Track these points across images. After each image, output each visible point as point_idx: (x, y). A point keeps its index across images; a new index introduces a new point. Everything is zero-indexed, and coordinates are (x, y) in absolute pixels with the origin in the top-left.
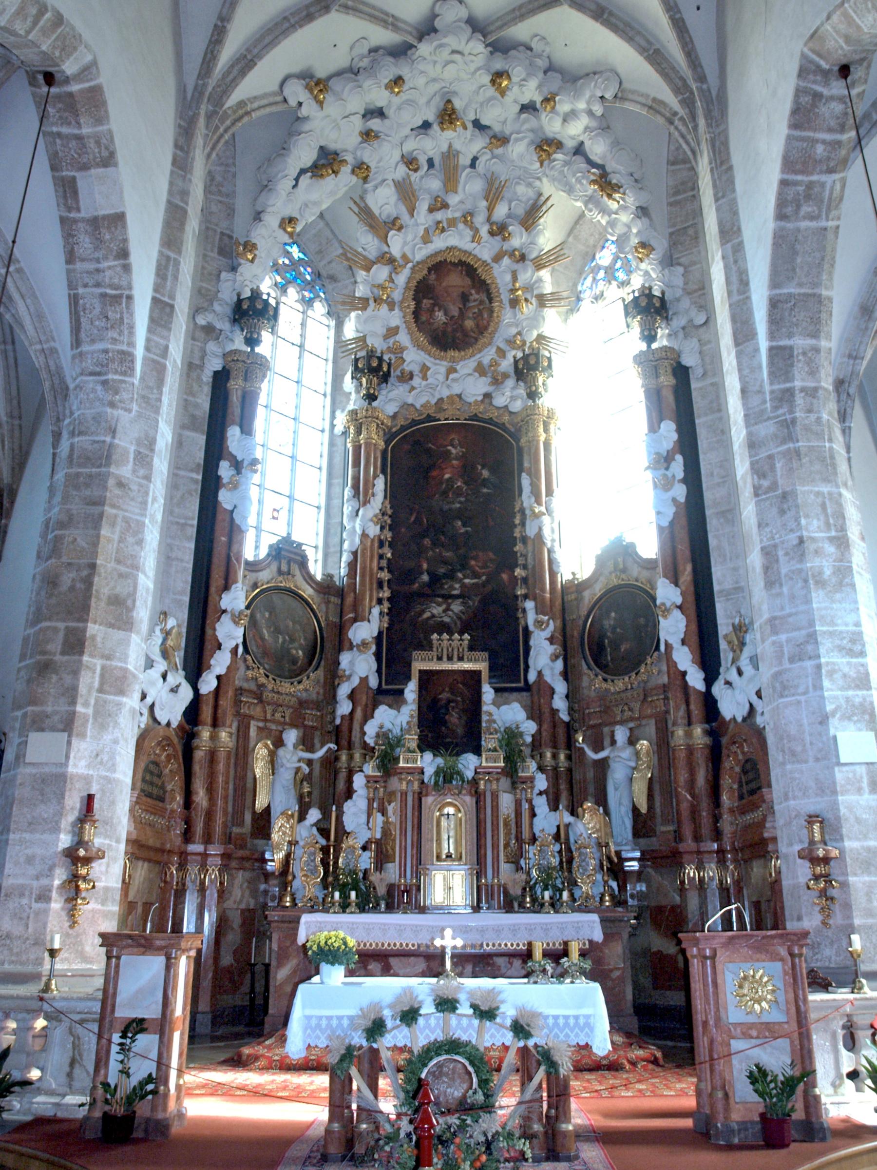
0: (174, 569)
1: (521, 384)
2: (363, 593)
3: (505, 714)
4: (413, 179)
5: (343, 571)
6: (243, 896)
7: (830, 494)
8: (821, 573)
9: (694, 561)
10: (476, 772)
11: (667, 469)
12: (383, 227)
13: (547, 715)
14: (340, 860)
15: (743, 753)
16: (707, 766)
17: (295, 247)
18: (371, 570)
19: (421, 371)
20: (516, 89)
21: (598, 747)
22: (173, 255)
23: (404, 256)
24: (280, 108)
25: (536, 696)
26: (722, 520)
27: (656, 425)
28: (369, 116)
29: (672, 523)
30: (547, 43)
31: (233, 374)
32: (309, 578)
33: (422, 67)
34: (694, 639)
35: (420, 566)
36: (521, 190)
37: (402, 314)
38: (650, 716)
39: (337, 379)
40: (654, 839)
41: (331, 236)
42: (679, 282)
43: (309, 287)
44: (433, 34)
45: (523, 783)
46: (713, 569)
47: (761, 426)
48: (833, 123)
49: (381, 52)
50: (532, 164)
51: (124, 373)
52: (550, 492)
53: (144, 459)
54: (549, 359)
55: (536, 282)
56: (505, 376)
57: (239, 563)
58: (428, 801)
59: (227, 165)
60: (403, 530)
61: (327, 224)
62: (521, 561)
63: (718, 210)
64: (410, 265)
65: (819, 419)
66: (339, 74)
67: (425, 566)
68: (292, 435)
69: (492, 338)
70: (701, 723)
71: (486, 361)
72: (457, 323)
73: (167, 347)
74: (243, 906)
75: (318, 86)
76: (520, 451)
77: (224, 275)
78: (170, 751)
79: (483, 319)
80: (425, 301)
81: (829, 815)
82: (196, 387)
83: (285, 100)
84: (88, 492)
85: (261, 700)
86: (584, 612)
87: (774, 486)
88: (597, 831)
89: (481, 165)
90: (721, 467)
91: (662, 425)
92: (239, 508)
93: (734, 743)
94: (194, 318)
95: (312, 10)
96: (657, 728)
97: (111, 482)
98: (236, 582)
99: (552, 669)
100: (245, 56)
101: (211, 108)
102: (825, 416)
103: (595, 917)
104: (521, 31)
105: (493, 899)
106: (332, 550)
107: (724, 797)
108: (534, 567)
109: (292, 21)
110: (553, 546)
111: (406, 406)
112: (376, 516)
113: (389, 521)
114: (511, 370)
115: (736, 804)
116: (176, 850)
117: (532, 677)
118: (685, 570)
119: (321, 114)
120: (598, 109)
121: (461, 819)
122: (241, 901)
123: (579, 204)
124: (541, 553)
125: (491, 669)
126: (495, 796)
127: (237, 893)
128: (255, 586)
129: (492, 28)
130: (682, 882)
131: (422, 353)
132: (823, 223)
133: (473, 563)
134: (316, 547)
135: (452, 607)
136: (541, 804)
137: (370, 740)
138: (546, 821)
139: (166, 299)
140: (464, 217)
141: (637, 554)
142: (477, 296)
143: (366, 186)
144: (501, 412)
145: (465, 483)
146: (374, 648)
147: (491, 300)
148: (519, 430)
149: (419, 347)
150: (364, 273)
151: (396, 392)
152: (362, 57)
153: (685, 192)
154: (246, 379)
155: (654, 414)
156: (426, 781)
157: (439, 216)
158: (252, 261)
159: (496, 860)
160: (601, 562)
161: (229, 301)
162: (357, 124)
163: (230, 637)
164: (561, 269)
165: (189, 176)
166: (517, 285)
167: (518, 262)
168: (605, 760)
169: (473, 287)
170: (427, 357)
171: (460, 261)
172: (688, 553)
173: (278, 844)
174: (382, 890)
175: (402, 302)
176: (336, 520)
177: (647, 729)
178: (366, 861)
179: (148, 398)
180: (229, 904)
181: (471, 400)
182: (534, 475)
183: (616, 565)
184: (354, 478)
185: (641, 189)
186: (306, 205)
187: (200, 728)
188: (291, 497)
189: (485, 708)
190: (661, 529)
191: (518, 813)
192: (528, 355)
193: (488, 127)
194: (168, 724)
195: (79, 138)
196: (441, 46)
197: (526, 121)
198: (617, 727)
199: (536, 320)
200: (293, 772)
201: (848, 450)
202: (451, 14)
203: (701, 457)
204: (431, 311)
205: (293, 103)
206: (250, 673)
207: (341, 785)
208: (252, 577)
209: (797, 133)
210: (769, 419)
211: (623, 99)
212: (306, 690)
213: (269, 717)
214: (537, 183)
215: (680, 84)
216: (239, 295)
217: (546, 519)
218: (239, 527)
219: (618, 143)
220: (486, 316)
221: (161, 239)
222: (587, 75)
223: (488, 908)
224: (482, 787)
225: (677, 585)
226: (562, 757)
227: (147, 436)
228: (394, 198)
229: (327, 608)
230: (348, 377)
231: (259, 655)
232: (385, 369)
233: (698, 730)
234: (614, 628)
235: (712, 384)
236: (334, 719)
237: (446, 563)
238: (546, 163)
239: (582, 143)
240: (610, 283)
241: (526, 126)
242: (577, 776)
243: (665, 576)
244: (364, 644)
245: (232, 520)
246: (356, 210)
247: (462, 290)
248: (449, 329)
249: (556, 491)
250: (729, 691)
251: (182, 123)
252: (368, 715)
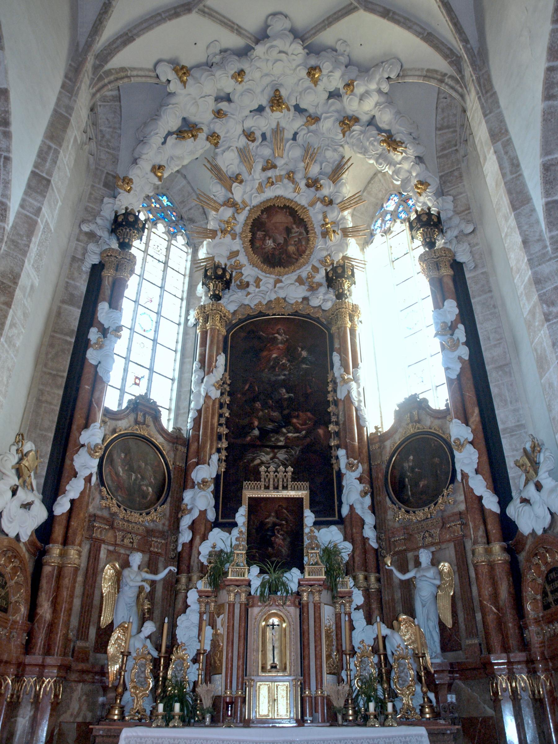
0: (43, 409)
1: (331, 290)
2: (205, 442)
4: (251, 148)
5: (189, 426)
6: (80, 709)
9: (480, 404)
10: (300, 585)
11: (452, 334)
12: (229, 180)
13: (358, 539)
14: (170, 672)
15: (546, 563)
16: (509, 580)
17: (165, 198)
18: (212, 424)
19: (255, 282)
20: (325, 79)
21: (404, 569)
25: (350, 526)
26: (500, 373)
27: (441, 304)
28: (219, 100)
29: (459, 376)
30: (347, 45)
31: (107, 266)
32: (162, 431)
33: (258, 64)
34: (486, 468)
35: (253, 423)
36: (329, 154)
37: (241, 242)
38: (449, 541)
40: (460, 652)
41: (191, 191)
42: (450, 206)
43: (173, 225)
44: (266, 39)
45: (342, 597)
46: (497, 412)
47: (544, 265)
49: (229, 52)
50: (336, 135)
52: (356, 365)
55: (341, 219)
56: (320, 285)
58: (255, 611)
59: (114, 128)
60: (239, 396)
61: (189, 183)
62: (334, 419)
63: (487, 122)
64: (248, 208)
67: (256, 423)
68: (154, 324)
69: (309, 259)
70: (499, 541)
71: (304, 275)
72: (282, 248)
73: (40, 209)
74: (80, 719)
75: (183, 71)
76: (331, 337)
77: (106, 200)
78: (17, 563)
79: (302, 246)
80: (259, 233)
82: (76, 274)
83: (158, 77)
85: (112, 527)
86: (386, 457)
88: (413, 642)
89: (300, 138)
90: (495, 332)
91: (446, 303)
92: (102, 363)
93: (536, 555)
94: (80, 226)
95: (178, 10)
96: (456, 551)
98: (94, 421)
99: (362, 504)
100: (127, 34)
101: (97, 62)
103: (422, 731)
104: (327, 37)
105: (316, 711)
106: (182, 411)
107: (529, 607)
108: (345, 421)
109: (163, 16)
110: (359, 405)
111: (243, 306)
112: (217, 382)
113: (228, 389)
114: (324, 281)
115: (541, 615)
116: (14, 661)
117: (345, 511)
118: (474, 412)
120: (385, 87)
121: (285, 629)
122: (78, 714)
123: (372, 161)
124: (350, 410)
125: (312, 494)
126: (317, 608)
127: (75, 706)
128: (114, 431)
130: (496, 693)
131: (256, 269)
133: (295, 420)
134: (169, 410)
135: (278, 455)
136: (359, 618)
137: (204, 559)
138: (364, 634)
139: (44, 175)
140: (288, 174)
141: (429, 407)
142: (297, 230)
143: (217, 150)
144: (316, 310)
145: (289, 361)
146: (212, 487)
147: (307, 232)
148: (330, 323)
149: (254, 265)
150: (214, 213)
151: (236, 296)
152: (215, 55)
153: (450, 148)
154: (117, 270)
155: (438, 296)
156: (252, 593)
157: (270, 173)
158: (129, 191)
159: (319, 669)
160: (399, 415)
161: (109, 218)
162: (211, 104)
163: (85, 467)
164: (358, 215)
165: (74, 98)
166: (327, 220)
167: (327, 205)
169: (295, 223)
170: (260, 272)
171: (285, 205)
173: (114, 656)
174: (207, 703)
175: (241, 234)
176: (186, 389)
177: (447, 552)
178: (193, 673)
179: (18, 243)
180: (66, 717)
181: (292, 302)
182: (343, 351)
183: (411, 418)
184: (201, 355)
185: (418, 144)
186: (172, 158)
187: (51, 545)
188: (151, 370)
189: (306, 530)
190: (450, 382)
191: (338, 627)
192: (336, 267)
193: (306, 110)
194: (18, 537)
196: (272, 47)
197: (333, 104)
198: (422, 550)
199: (343, 246)
200: (137, 590)
202: (278, 25)
203: (478, 326)
204: (263, 240)
205: (163, 79)
206: (104, 503)
208: (111, 424)
210: (551, 259)
211: (404, 76)
212: (153, 521)
213: (118, 542)
214: (341, 149)
215: (448, 52)
216: (116, 212)
217: (353, 385)
218: (101, 378)
219: (400, 113)
220: (304, 243)
221: (46, 133)
222: (377, 65)
223: (312, 722)
224: (305, 599)
225: (467, 425)
226: (373, 579)
227: (12, 272)
228: (237, 161)
229: (175, 455)
230: (200, 286)
231: (113, 489)
232: (228, 277)
233: (497, 547)
234: (412, 469)
235: (482, 273)
236: (177, 546)
237: (272, 421)
238: (347, 133)
239: (374, 116)
240: (395, 221)
241: (333, 108)
242: (386, 597)
243: (457, 417)
244: (204, 482)
245: (96, 372)
247: (285, 225)
248: (277, 252)
249: (361, 365)
250: (527, 508)
251: (73, 64)
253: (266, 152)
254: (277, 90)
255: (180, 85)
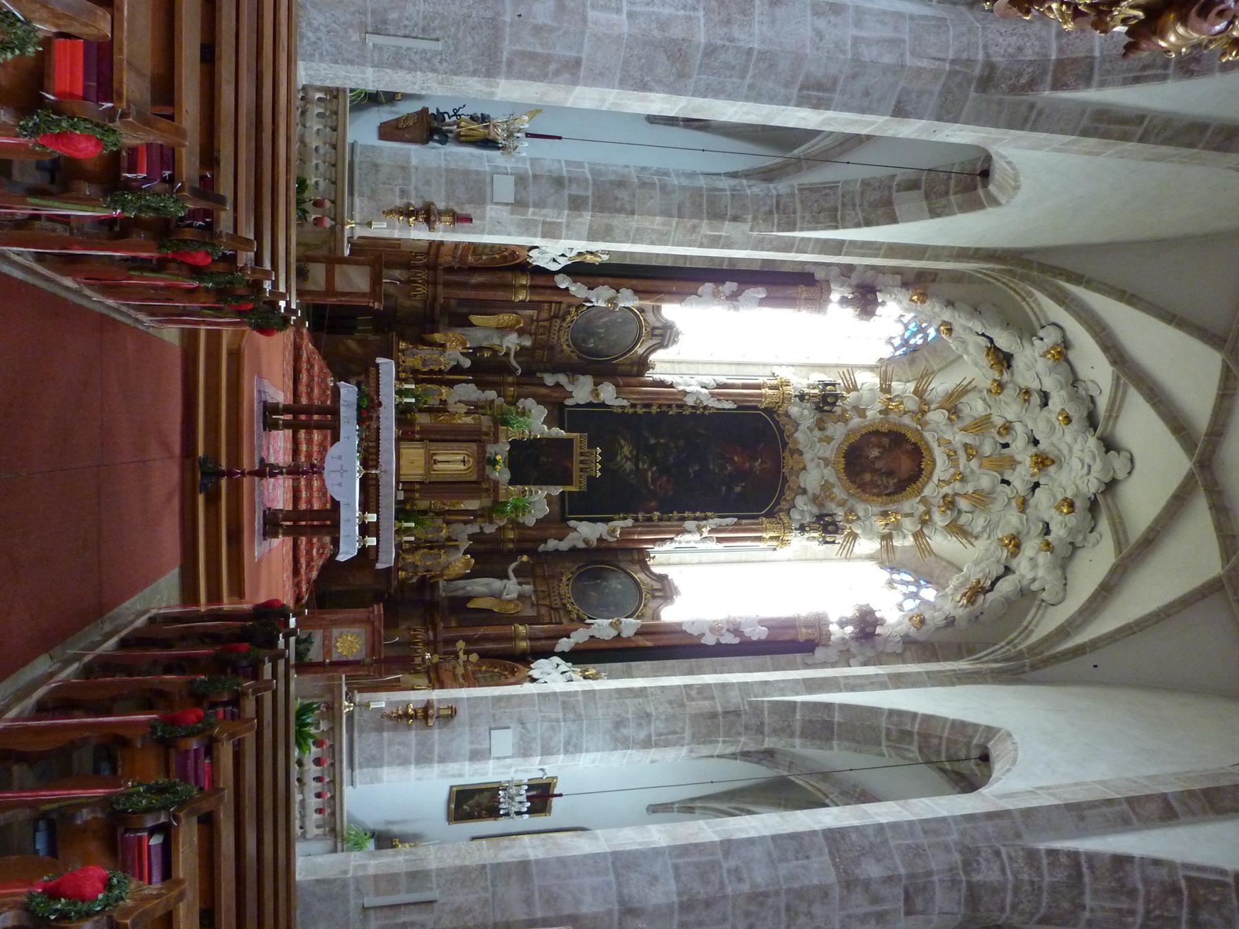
3: (539, 501)
7: (683, 738)
8: (625, 726)
20: (1060, 518)
21: (517, 573)
22: (882, 252)
23: (927, 423)
24: (1036, 323)
30: (1094, 546)
31: (811, 289)
32: (652, 350)
33: (1079, 440)
34: (593, 646)
39: (822, 367)
41: (949, 360)
48: (952, 751)
49: (1091, 406)
51: (779, 225)
52: (720, 540)
53: (714, 242)
54: (833, 542)
56: (821, 506)
57: (657, 301)
58: (474, 446)
62: (665, 516)
65: (739, 734)
66: (1073, 370)
81: (456, 720)
83: (1043, 327)
84: (688, 205)
87: (691, 699)
97: (696, 221)
98: (640, 299)
102: (742, 739)
111: (796, 425)
117: (572, 523)
119: (1037, 355)
124: (671, 532)
129: (1109, 500)
132: (884, 743)
133: (665, 478)
136: (474, 529)
147: (888, 495)
149: (847, 435)
152: (1086, 390)
154: (806, 299)
157: (961, 453)
160: (662, 578)
162: (1035, 385)
168: (507, 577)
169: (900, 481)
172: (661, 643)
190: (680, 624)
195: (947, 193)
199: (870, 533)
201: (718, 756)
202: (1118, 463)
204: (879, 445)
207: (490, 378)
209: (948, 725)
212: (562, 351)
214: (985, 536)
225: (636, 634)
246: (965, 383)
252: (540, 400)
253: (987, 449)
254: (1053, 462)
255: (1041, 352)
